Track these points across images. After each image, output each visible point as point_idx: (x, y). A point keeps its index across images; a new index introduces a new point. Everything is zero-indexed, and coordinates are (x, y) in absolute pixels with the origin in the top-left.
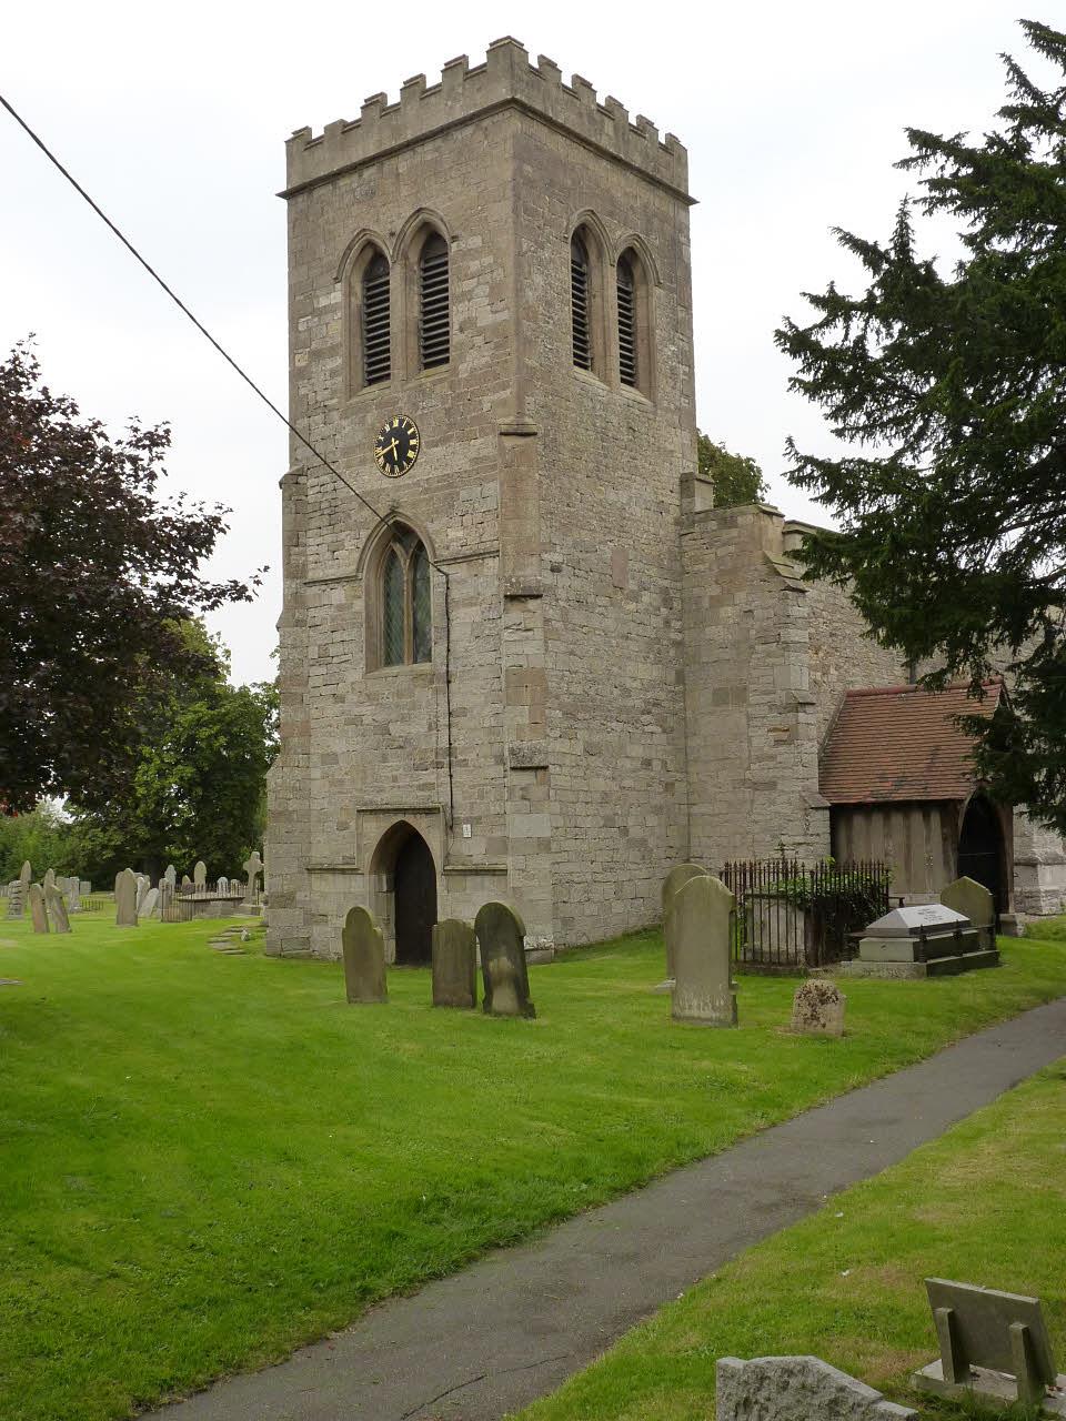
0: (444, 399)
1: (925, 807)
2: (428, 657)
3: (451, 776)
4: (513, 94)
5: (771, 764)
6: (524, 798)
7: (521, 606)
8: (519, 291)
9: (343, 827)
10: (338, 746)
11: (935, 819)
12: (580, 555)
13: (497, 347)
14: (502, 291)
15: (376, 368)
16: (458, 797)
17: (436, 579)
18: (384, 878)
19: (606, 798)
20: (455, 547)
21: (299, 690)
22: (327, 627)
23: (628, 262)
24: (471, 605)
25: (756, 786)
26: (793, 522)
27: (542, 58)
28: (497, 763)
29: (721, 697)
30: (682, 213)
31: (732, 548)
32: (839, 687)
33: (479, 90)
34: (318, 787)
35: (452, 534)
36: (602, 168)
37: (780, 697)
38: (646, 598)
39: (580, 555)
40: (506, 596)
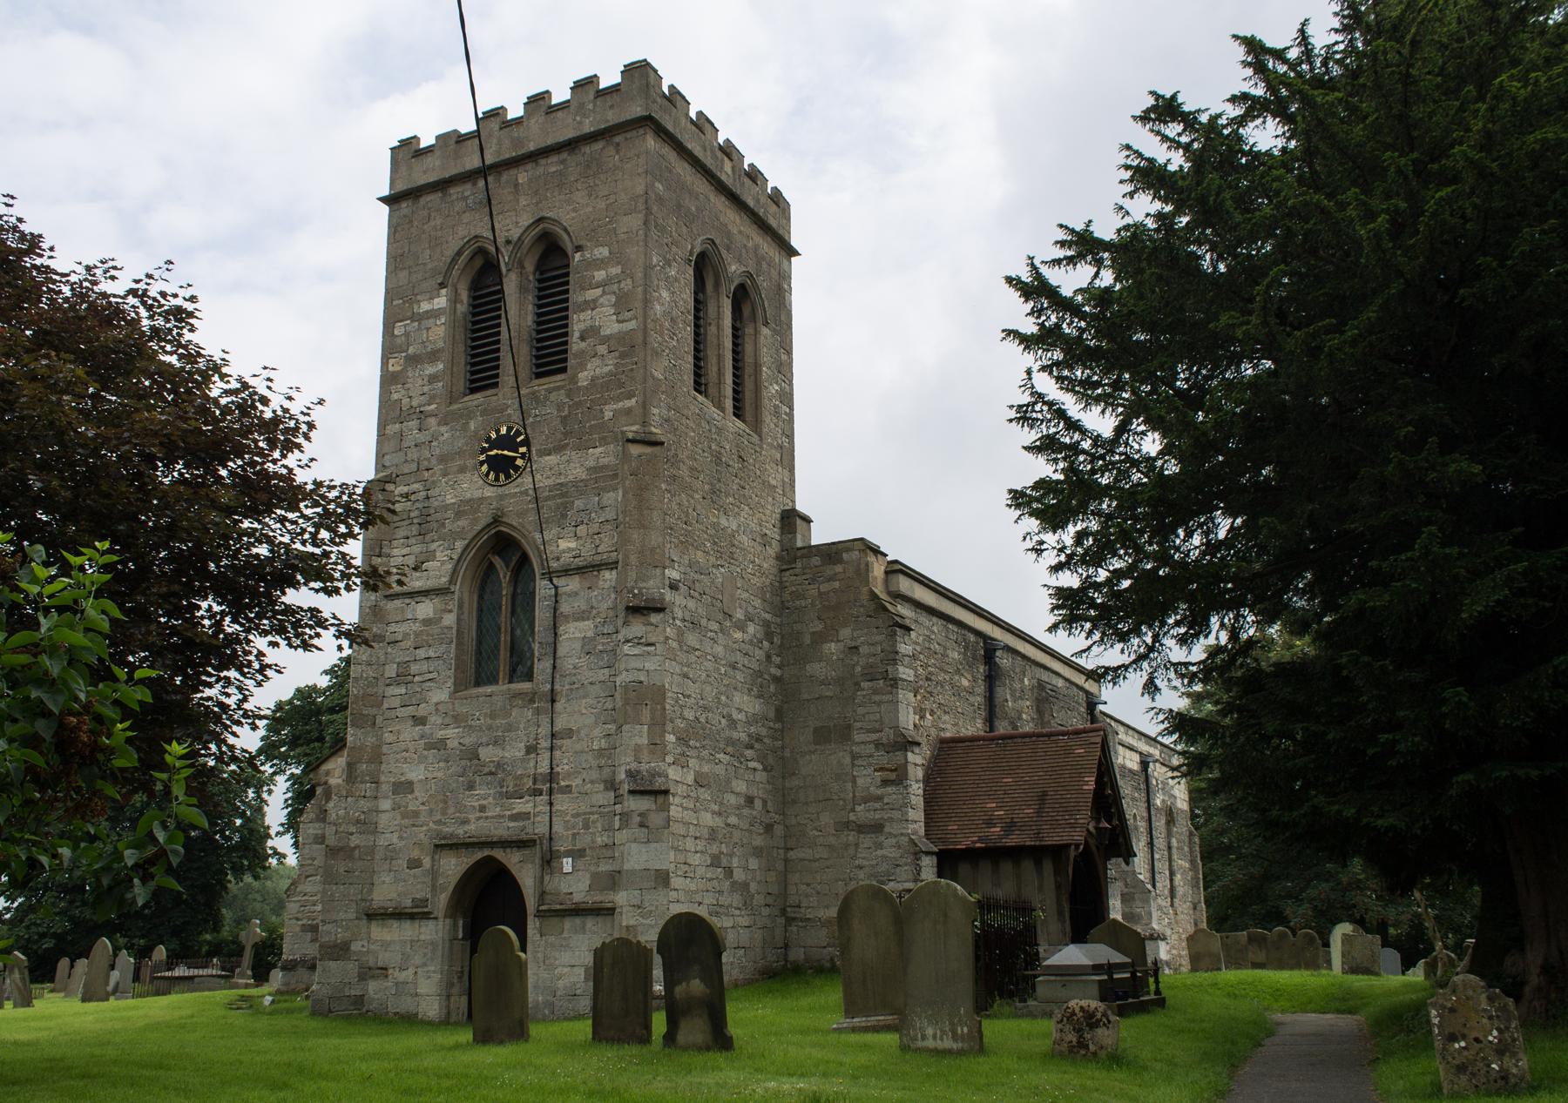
0: (560, 407)
1: (1036, 853)
2: (529, 676)
3: (551, 804)
4: (636, 117)
5: (877, 805)
6: (642, 825)
7: (642, 619)
8: (647, 302)
9: (414, 864)
10: (415, 774)
11: (1048, 867)
12: (697, 576)
13: (623, 356)
14: (627, 303)
15: (481, 372)
16: (558, 828)
17: (543, 588)
18: (461, 923)
19: (713, 835)
20: (566, 559)
21: (373, 711)
22: (408, 643)
23: (742, 296)
24: (583, 619)
25: (862, 829)
26: (896, 562)
27: (672, 87)
28: (606, 789)
29: (823, 736)
30: (785, 262)
31: (837, 584)
32: (933, 732)
33: (612, 107)
34: (387, 819)
35: (563, 544)
36: (719, 203)
37: (887, 735)
38: (751, 629)
39: (697, 576)
40: (628, 608)
